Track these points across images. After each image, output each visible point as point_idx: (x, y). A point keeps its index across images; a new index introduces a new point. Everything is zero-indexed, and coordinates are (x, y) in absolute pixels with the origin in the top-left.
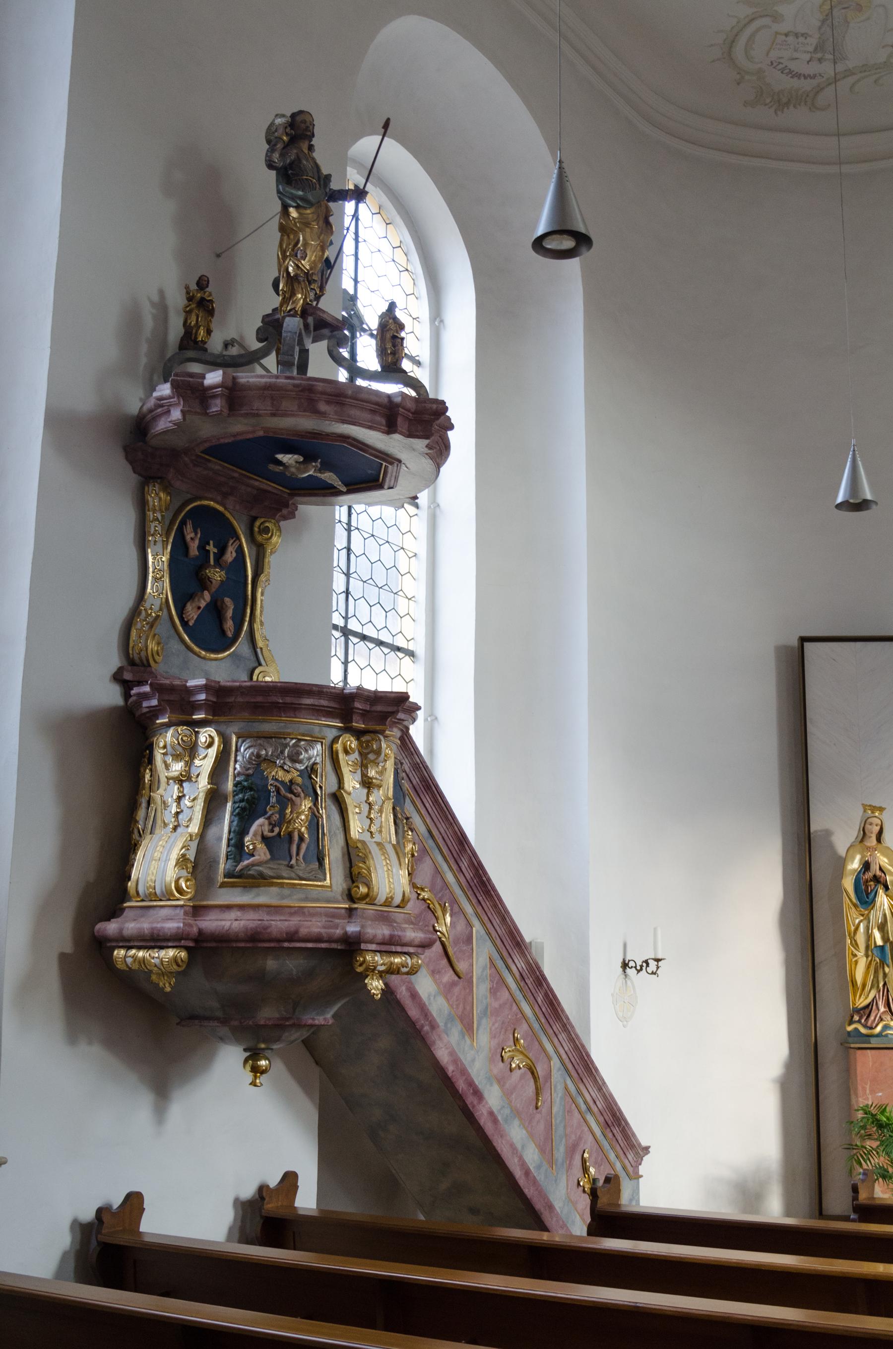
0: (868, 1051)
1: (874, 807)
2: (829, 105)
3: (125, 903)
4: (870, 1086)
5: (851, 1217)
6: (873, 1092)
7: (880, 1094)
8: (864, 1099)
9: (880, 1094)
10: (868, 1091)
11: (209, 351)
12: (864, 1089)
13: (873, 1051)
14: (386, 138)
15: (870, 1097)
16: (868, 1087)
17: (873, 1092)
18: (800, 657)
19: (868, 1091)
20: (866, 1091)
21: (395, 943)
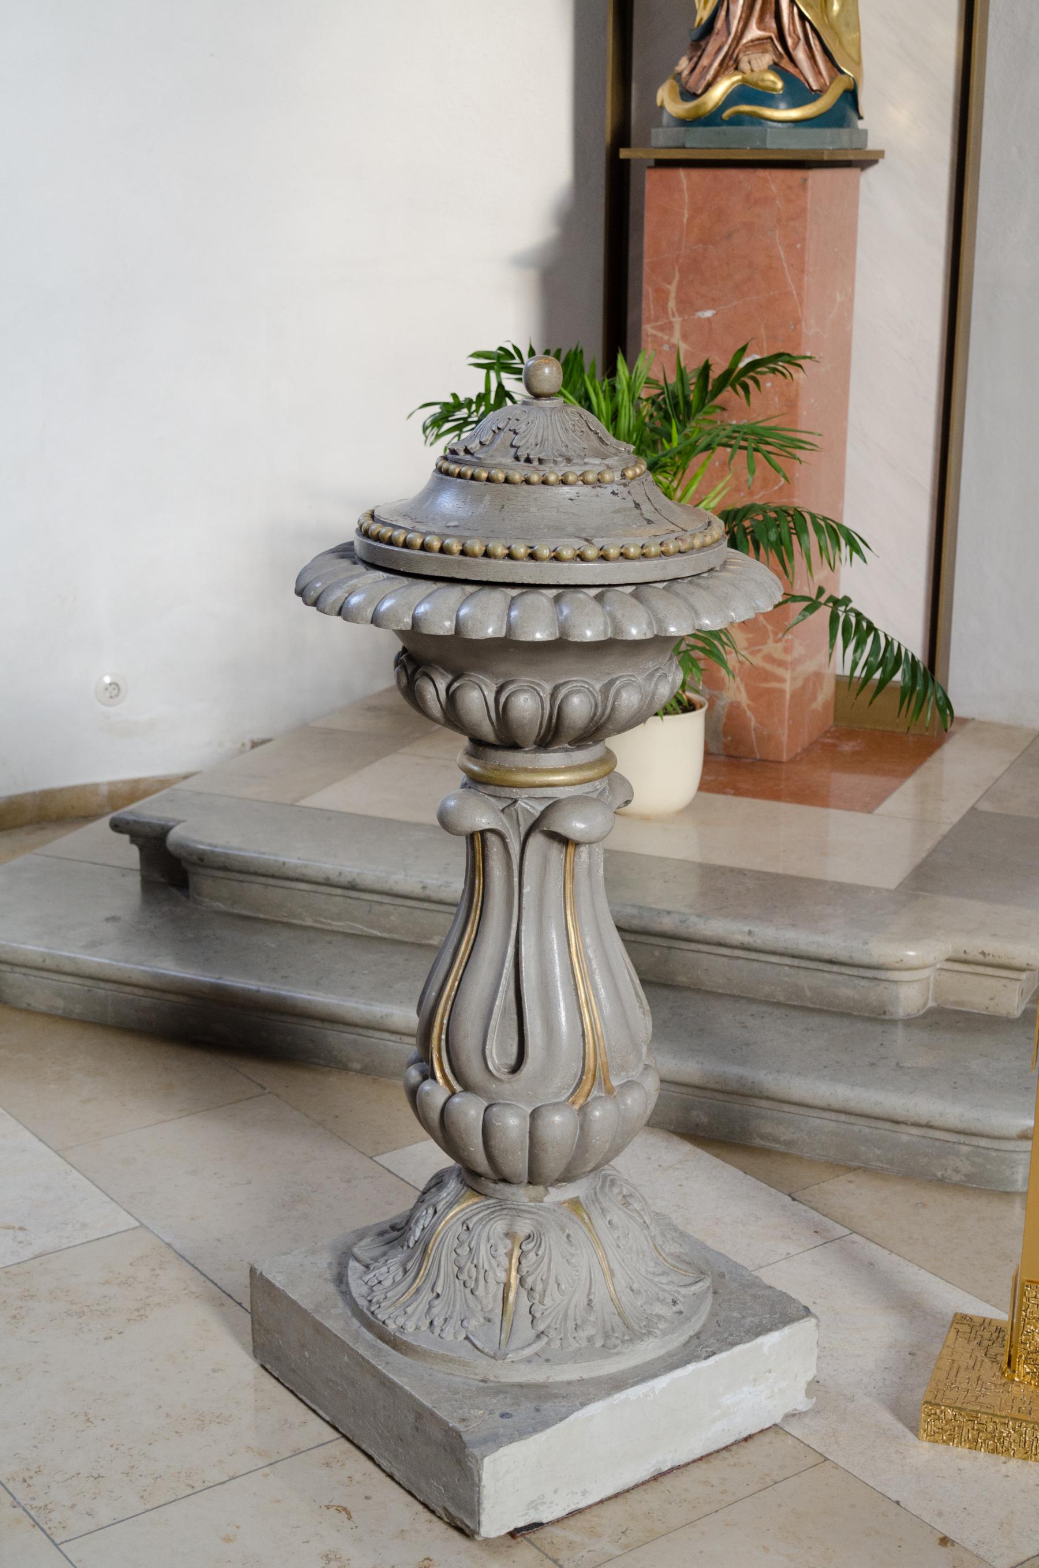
0: (682, 173)
1: (362, 1073)
2: (521, 1182)
3: (759, 367)
4: (680, 286)
5: (392, 918)
6: (686, 305)
7: (709, 314)
8: (661, 329)
9: (709, 314)
10: (672, 304)
11: (738, 450)
12: (662, 296)
13: (696, 174)
14: (799, 428)
15: (677, 320)
16: (673, 288)
17: (686, 305)
18: (485, 902)
19: (672, 304)
20: (666, 300)
21: (450, 830)
